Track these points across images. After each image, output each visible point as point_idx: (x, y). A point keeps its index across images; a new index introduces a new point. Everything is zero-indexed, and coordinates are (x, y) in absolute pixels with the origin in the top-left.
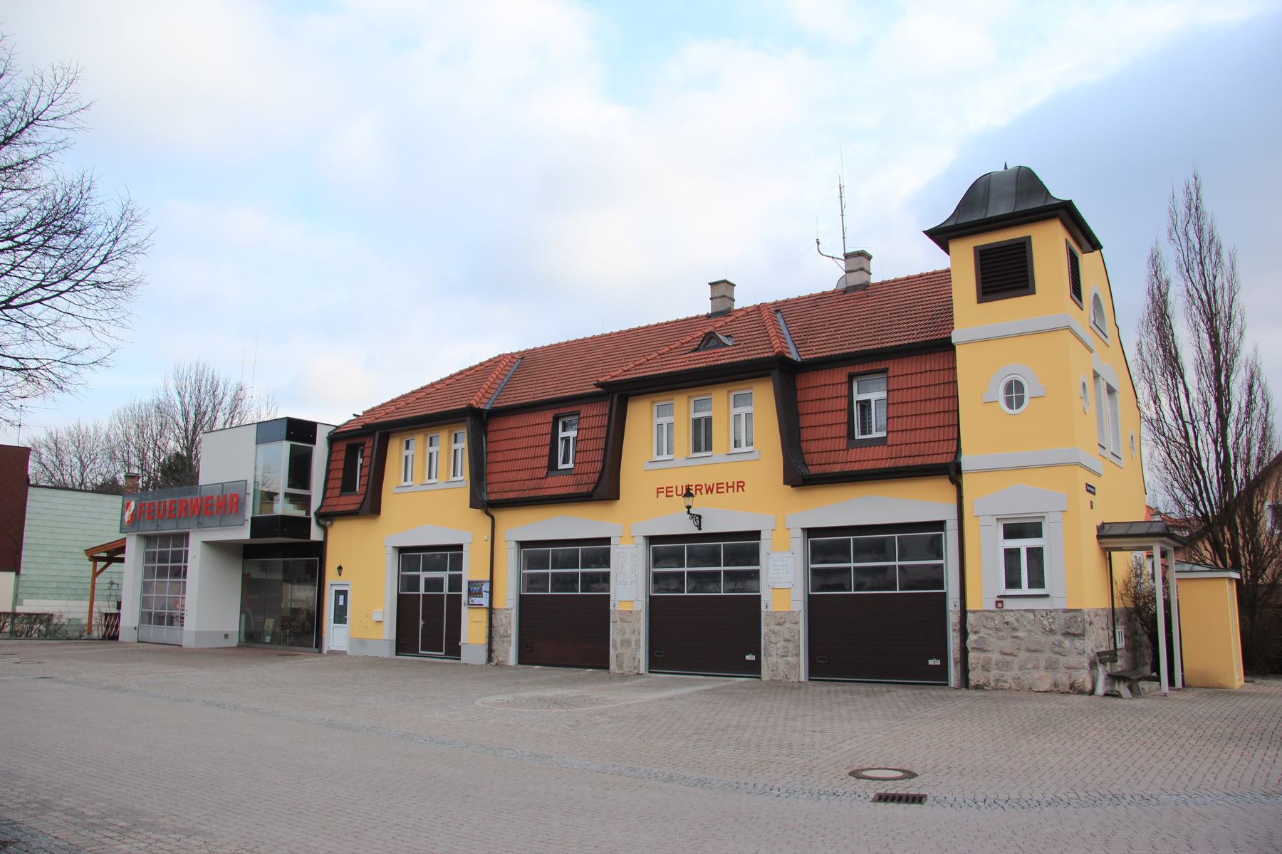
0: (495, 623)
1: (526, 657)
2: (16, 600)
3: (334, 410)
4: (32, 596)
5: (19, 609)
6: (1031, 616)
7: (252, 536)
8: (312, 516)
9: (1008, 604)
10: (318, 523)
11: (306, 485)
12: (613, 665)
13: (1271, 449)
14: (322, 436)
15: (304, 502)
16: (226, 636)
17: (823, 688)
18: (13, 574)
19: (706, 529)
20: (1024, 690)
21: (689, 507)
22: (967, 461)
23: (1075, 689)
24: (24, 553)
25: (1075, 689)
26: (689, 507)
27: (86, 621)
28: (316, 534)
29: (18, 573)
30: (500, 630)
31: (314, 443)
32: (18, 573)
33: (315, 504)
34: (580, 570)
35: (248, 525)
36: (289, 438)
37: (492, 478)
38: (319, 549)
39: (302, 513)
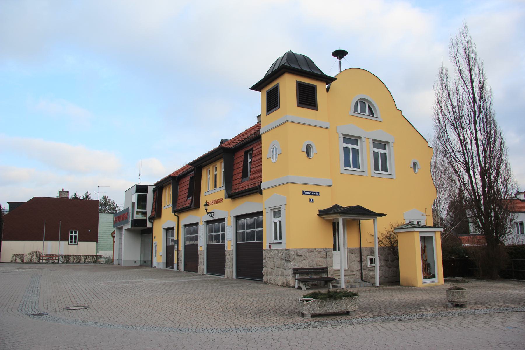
0: (179, 255)
1: (186, 269)
2: (97, 252)
3: (150, 182)
4: (102, 250)
5: (98, 254)
6: (277, 252)
7: (131, 227)
8: (147, 219)
9: (274, 247)
10: (149, 221)
11: (145, 207)
12: (198, 272)
13: (465, 282)
14: (150, 190)
15: (145, 214)
16: (135, 262)
17: (239, 281)
18: (95, 243)
19: (216, 217)
20: (276, 285)
21: (206, 210)
22: (263, 187)
23: (288, 285)
24: (99, 235)
25: (288, 285)
26: (206, 210)
27: (112, 258)
28: (149, 225)
29: (97, 242)
30: (180, 259)
31: (147, 192)
32: (97, 242)
33: (149, 215)
34: (255, 229)
35: (130, 223)
36: (137, 192)
37: (179, 202)
38: (151, 230)
39: (144, 218)
